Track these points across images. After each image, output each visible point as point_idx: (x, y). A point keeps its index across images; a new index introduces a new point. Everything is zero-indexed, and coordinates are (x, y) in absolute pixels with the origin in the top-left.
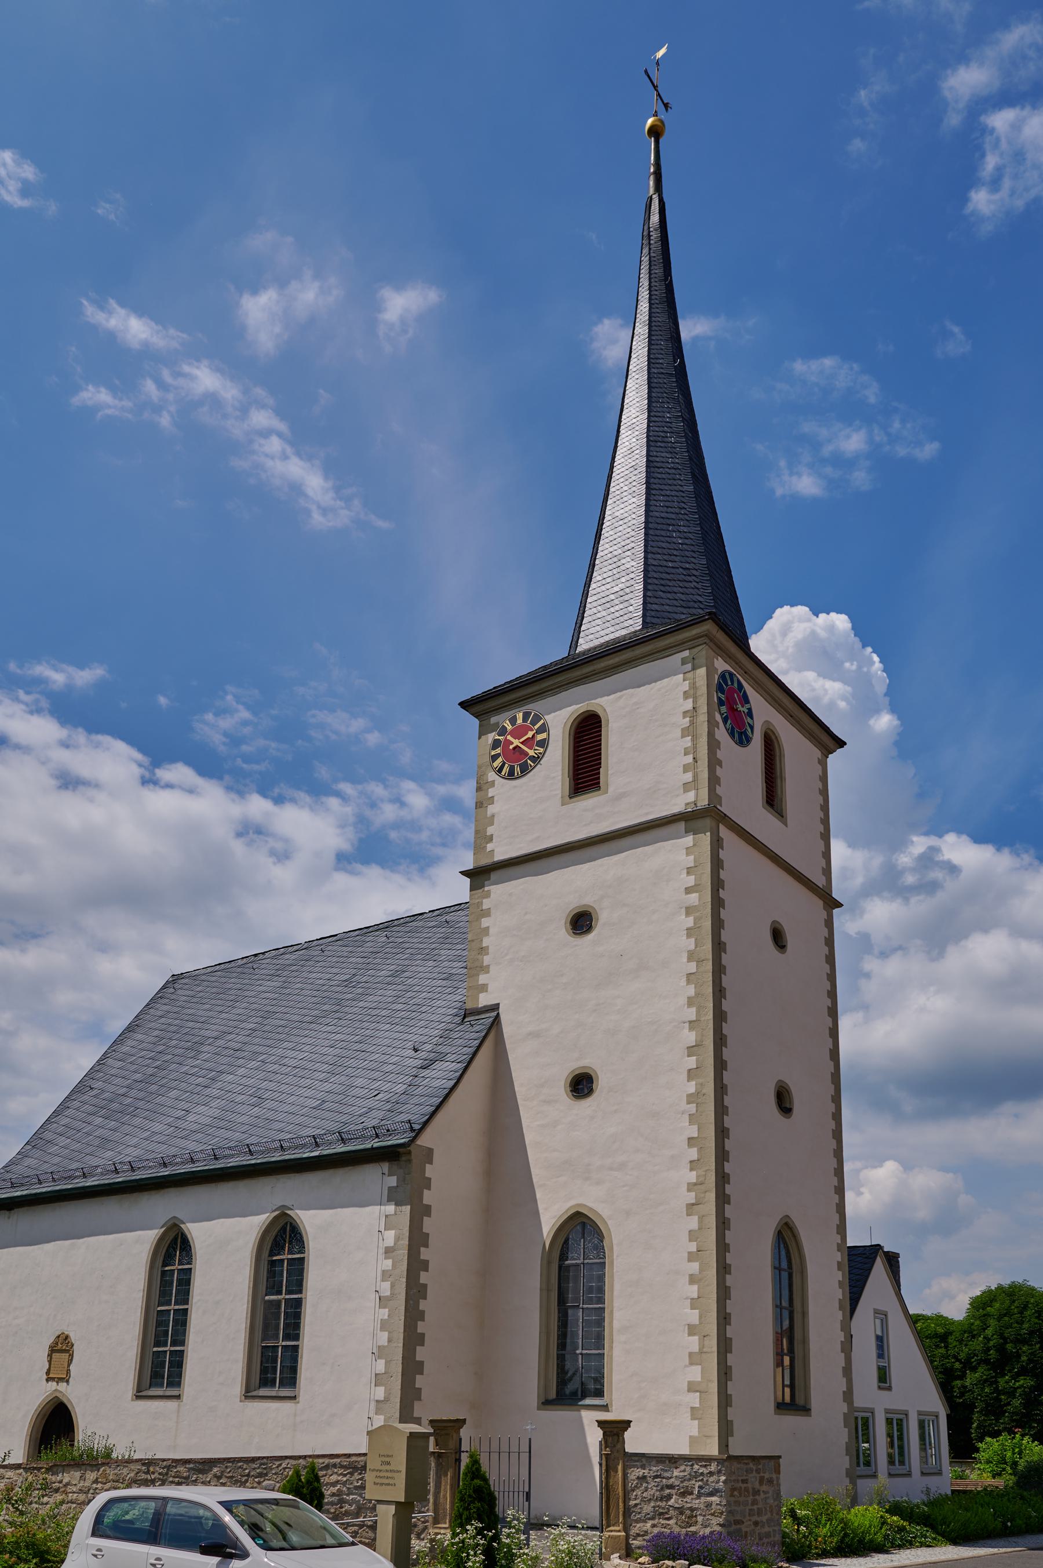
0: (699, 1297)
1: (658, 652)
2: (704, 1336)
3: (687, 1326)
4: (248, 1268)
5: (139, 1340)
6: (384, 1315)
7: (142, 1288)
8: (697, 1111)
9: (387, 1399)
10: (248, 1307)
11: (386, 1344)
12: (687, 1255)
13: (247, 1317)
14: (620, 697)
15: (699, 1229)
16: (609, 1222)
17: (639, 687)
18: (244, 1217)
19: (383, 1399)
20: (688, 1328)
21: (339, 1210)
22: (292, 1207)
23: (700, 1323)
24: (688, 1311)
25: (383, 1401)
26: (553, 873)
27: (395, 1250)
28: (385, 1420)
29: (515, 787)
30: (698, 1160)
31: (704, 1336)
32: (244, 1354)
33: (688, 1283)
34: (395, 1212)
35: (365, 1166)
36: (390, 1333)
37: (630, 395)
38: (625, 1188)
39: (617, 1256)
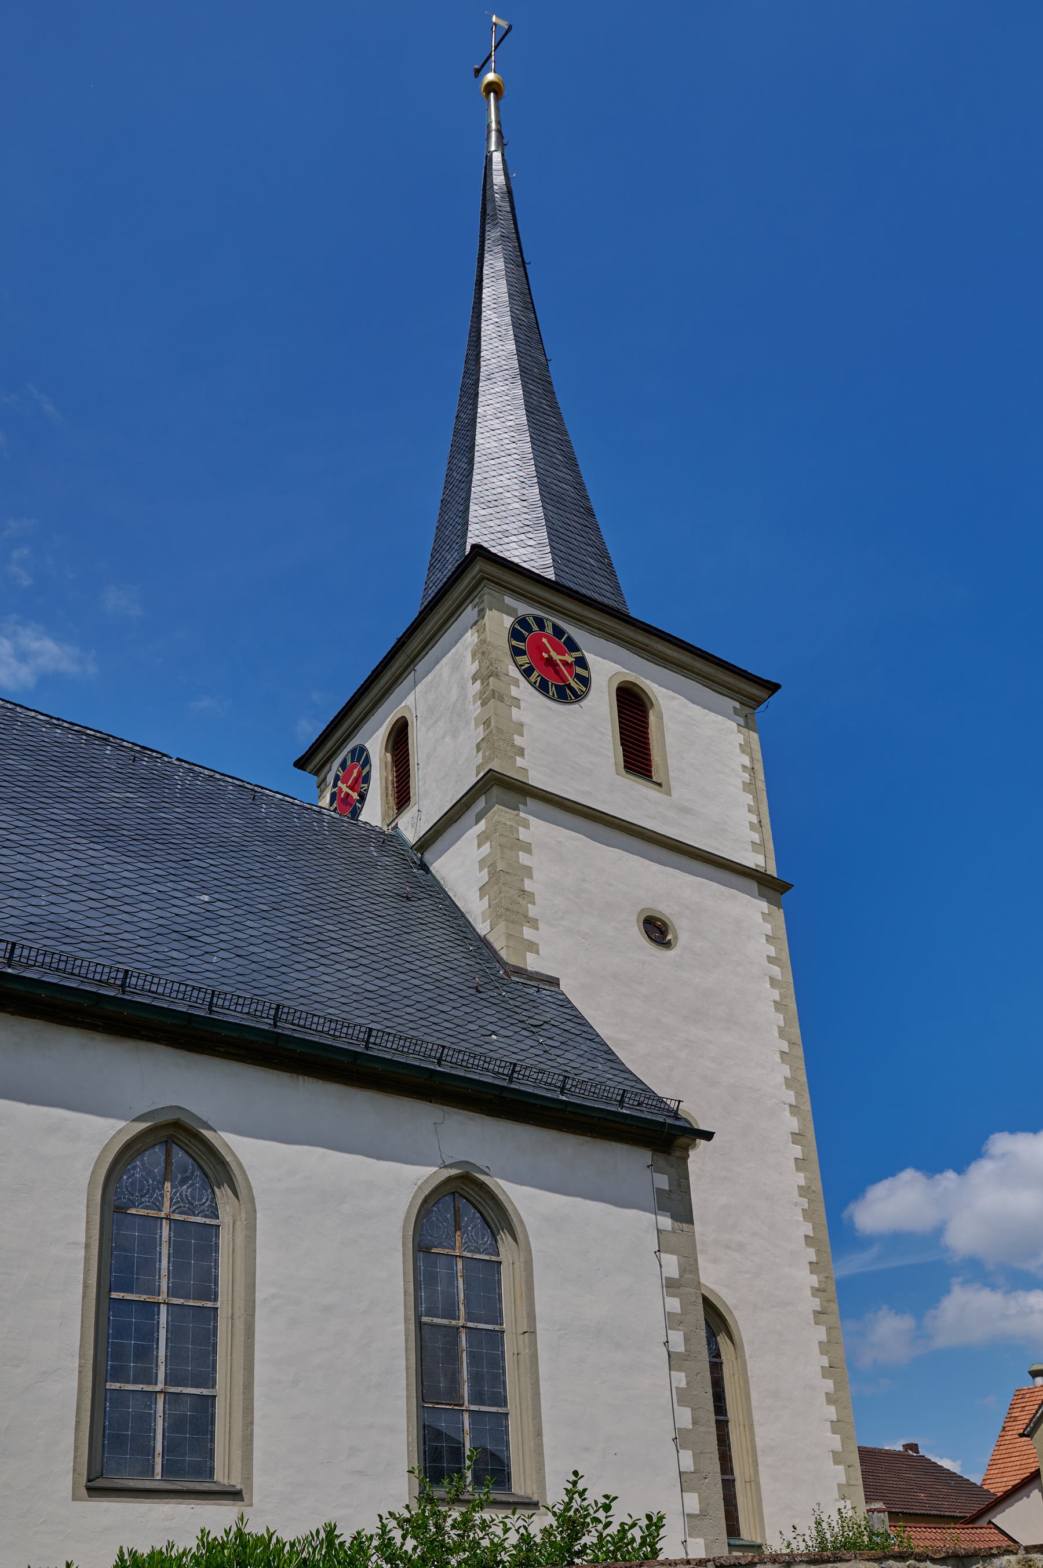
0: (838, 1421)
1: (713, 681)
2: (849, 1467)
3: (831, 1453)
4: (399, 1256)
5: (82, 1356)
6: (680, 1381)
7: (82, 1239)
8: (809, 1207)
9: (703, 1514)
10: (407, 1330)
11: (690, 1427)
12: (820, 1369)
13: (407, 1349)
14: (674, 698)
15: (828, 1342)
16: (735, 1313)
17: (693, 703)
18: (378, 1159)
19: (698, 1512)
20: (833, 1456)
21: (578, 1200)
22: (487, 1170)
23: (844, 1451)
24: (829, 1434)
25: (698, 1515)
26: (619, 850)
27: (682, 1285)
28: (707, 1547)
29: (550, 709)
30: (817, 1263)
31: (849, 1467)
32: (408, 1418)
33: (825, 1402)
34: (673, 1228)
35: (614, 1144)
36: (693, 1410)
37: (487, 329)
38: (747, 1275)
39: (750, 1357)
